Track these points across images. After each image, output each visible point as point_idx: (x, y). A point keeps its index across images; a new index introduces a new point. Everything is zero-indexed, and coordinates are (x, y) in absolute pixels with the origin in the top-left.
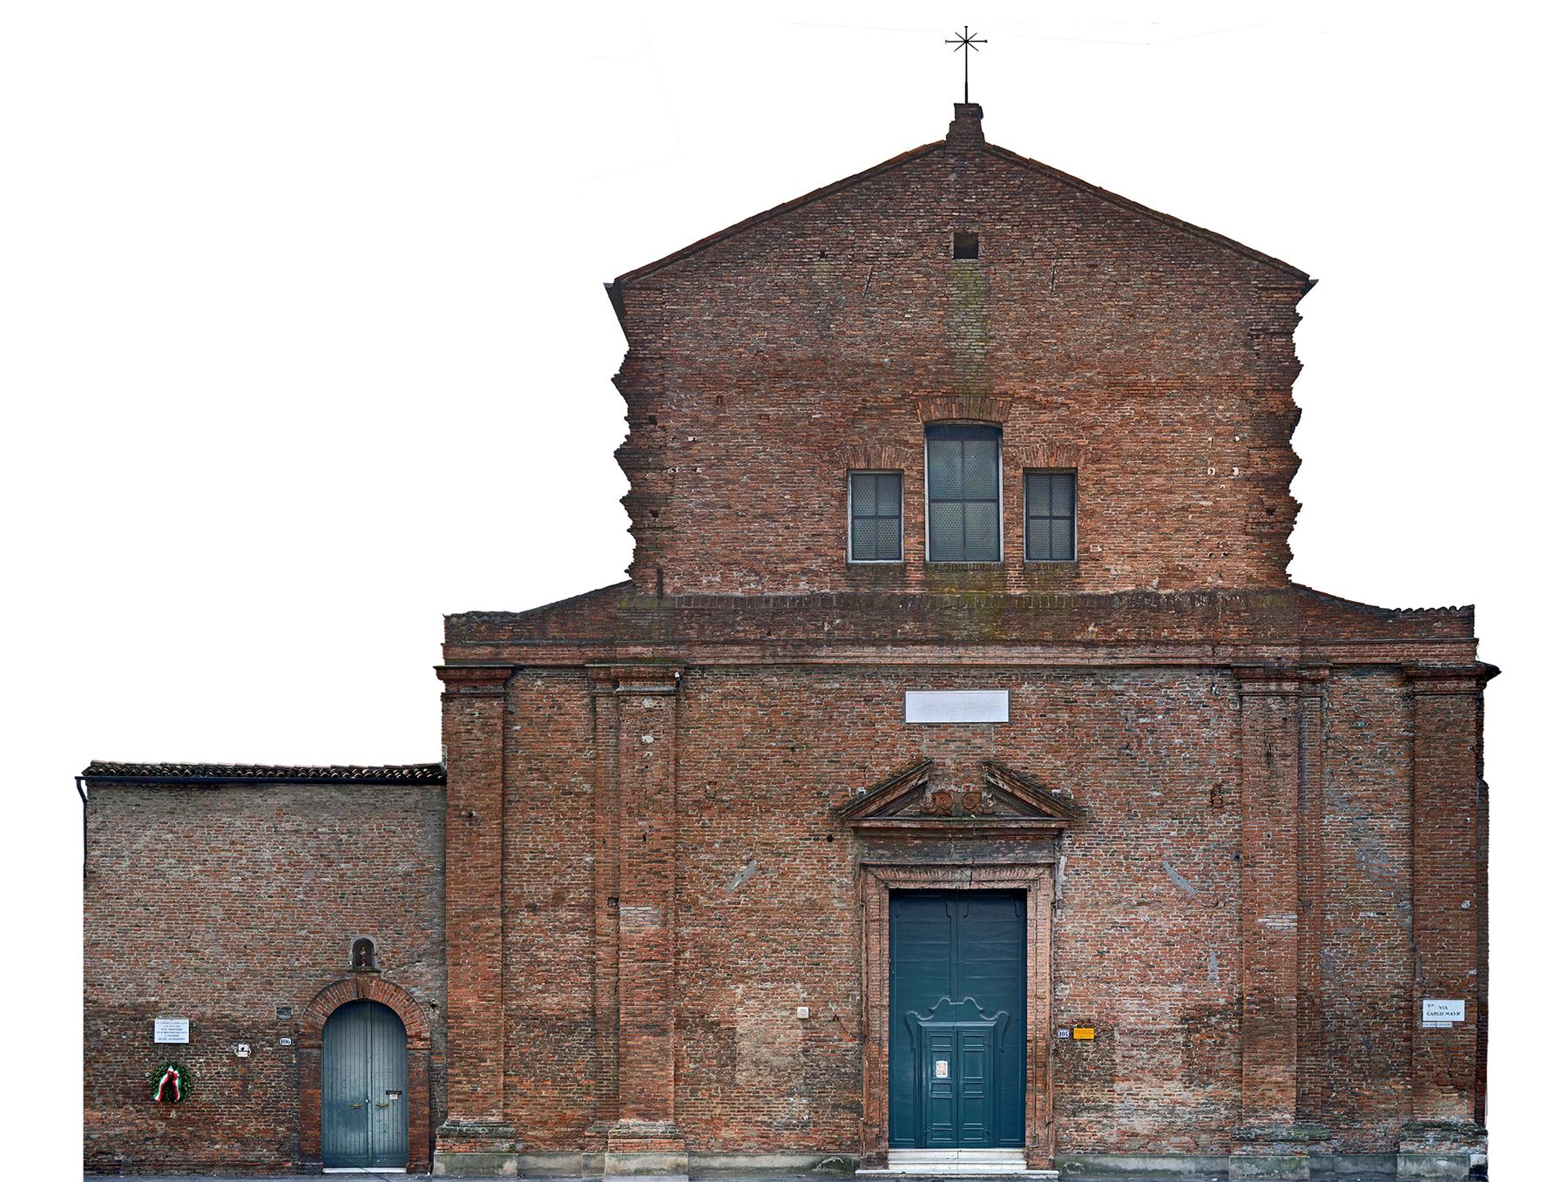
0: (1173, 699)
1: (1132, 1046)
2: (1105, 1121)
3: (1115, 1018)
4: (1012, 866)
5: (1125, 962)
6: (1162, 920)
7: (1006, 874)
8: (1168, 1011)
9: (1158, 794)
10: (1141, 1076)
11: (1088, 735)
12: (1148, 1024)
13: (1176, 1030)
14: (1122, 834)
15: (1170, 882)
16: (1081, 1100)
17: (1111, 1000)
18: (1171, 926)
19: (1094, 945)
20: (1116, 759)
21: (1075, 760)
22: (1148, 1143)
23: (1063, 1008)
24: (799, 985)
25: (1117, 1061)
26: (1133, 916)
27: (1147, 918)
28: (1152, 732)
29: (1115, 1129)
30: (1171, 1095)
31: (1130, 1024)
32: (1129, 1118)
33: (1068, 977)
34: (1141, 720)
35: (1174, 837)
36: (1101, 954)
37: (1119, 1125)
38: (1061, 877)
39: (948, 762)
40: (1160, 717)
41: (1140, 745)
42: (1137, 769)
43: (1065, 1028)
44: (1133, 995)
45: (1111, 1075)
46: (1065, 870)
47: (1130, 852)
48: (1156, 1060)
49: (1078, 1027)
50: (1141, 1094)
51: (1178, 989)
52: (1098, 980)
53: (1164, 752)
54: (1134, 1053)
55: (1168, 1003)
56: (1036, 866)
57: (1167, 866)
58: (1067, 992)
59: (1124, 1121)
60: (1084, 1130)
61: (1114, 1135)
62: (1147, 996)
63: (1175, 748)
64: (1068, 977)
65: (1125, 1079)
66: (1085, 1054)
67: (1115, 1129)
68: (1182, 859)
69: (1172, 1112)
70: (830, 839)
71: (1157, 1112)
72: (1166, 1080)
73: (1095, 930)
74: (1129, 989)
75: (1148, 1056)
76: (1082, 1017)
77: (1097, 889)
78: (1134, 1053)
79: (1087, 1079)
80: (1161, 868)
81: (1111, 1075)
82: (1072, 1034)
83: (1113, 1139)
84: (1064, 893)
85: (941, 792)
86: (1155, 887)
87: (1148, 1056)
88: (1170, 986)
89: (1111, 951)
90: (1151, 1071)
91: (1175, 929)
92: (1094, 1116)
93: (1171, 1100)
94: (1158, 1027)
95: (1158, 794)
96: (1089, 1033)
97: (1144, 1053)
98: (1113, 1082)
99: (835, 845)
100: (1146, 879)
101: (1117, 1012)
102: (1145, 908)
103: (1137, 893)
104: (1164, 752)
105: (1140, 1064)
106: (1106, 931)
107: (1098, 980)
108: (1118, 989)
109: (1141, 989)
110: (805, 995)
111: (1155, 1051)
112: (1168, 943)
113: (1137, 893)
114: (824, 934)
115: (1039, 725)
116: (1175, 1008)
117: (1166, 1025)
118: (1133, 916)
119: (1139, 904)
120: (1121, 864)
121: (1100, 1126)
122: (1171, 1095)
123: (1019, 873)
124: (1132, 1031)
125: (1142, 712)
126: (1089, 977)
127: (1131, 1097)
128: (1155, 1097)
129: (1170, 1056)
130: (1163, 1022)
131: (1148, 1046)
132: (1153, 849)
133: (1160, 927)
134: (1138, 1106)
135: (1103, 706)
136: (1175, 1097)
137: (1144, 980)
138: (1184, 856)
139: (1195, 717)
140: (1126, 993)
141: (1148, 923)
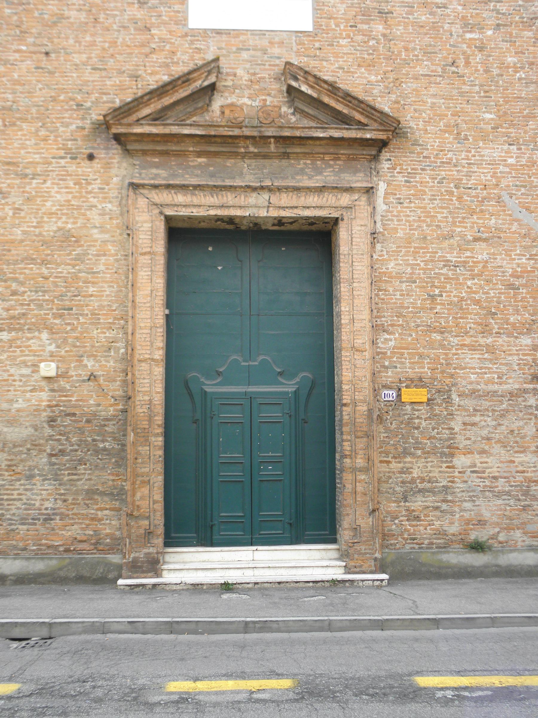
0: (503, 14)
1: (475, 410)
2: (444, 506)
3: (452, 376)
4: (321, 190)
5: (461, 309)
6: (503, 259)
7: (313, 200)
8: (516, 368)
9: (492, 116)
10: (487, 448)
11: (406, 49)
12: (493, 383)
13: (525, 391)
14: (451, 159)
15: (510, 215)
16: (413, 481)
17: (446, 354)
18: (515, 266)
19: (424, 287)
20: (440, 76)
21: (392, 76)
22: (498, 532)
23: (387, 363)
24: (45, 335)
25: (457, 429)
26: (468, 254)
27: (485, 256)
28: (481, 49)
29: (457, 516)
30: (523, 472)
31: (471, 383)
32: (474, 501)
33: (392, 325)
34: (468, 36)
35: (512, 165)
36: (432, 297)
37: (461, 511)
38: (381, 207)
39: (240, 72)
40: (490, 33)
41: (467, 63)
42: (466, 88)
43: (390, 388)
44: (473, 348)
45: (449, 447)
46: (385, 198)
47: (461, 180)
48: (503, 428)
49: (407, 387)
50: (488, 471)
51: (526, 341)
52: (431, 329)
53: (496, 72)
54: (477, 419)
55: (516, 357)
56: (349, 190)
57: (506, 197)
58: (392, 344)
59: (467, 505)
60: (417, 518)
61: (456, 524)
62: (490, 349)
63: (508, 67)
64: (392, 325)
65: (469, 452)
66: (417, 421)
67: (457, 516)
68: (523, 190)
69: (526, 493)
70: (91, 157)
71: (508, 493)
72: (516, 452)
73: (423, 269)
74: (468, 341)
75: (494, 423)
76: (412, 375)
77: (424, 221)
78: (477, 419)
79: (419, 452)
80: (499, 200)
81: (449, 447)
82: (399, 396)
83: (454, 529)
84: (383, 225)
85: (232, 105)
86: (493, 221)
87: (494, 423)
88: (516, 337)
89: (444, 294)
90: (499, 441)
91: (519, 270)
92: (430, 500)
93: (525, 478)
94: (505, 387)
95: (492, 116)
96: (422, 395)
97: (489, 419)
98: (452, 455)
99: (96, 164)
100: (482, 211)
101: (455, 368)
102: (484, 245)
103: (472, 227)
104: (496, 72)
105: (484, 433)
106: (437, 271)
107: (431, 329)
108: (456, 340)
109: (482, 341)
110: (52, 348)
111: (502, 416)
112: (511, 286)
113: (472, 227)
114: (80, 271)
115: (348, 36)
116: (525, 365)
117: (512, 385)
118: (468, 254)
119: (476, 240)
120: (451, 193)
121: (438, 513)
122: (523, 472)
123: (329, 199)
124: (474, 391)
125: (468, 26)
126: (418, 326)
127: (475, 475)
128: (505, 475)
129: (521, 423)
130: (511, 381)
131: (494, 410)
132: (489, 178)
133: (501, 267)
134: (485, 486)
135: (423, 18)
136: (529, 475)
137: (486, 330)
138: (525, 187)
139: (530, 34)
140: (464, 345)
141: (486, 262)
